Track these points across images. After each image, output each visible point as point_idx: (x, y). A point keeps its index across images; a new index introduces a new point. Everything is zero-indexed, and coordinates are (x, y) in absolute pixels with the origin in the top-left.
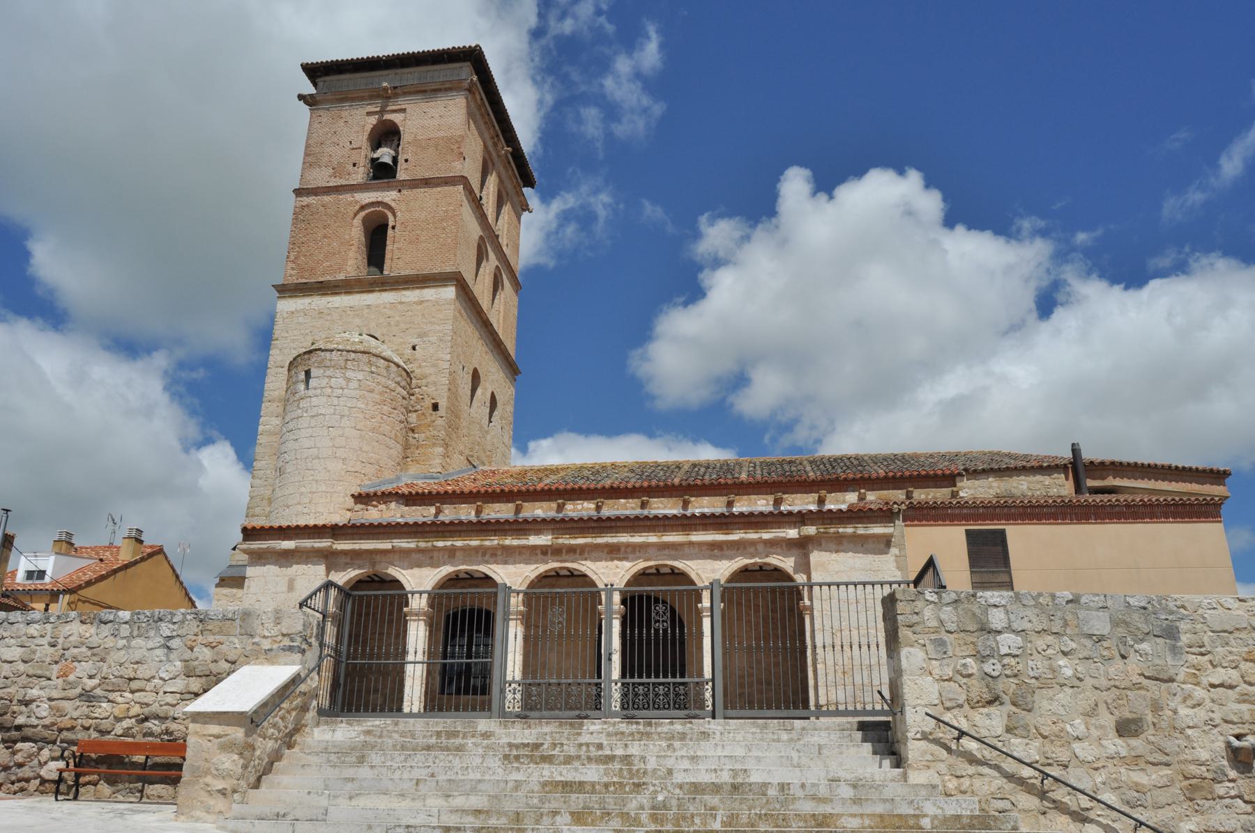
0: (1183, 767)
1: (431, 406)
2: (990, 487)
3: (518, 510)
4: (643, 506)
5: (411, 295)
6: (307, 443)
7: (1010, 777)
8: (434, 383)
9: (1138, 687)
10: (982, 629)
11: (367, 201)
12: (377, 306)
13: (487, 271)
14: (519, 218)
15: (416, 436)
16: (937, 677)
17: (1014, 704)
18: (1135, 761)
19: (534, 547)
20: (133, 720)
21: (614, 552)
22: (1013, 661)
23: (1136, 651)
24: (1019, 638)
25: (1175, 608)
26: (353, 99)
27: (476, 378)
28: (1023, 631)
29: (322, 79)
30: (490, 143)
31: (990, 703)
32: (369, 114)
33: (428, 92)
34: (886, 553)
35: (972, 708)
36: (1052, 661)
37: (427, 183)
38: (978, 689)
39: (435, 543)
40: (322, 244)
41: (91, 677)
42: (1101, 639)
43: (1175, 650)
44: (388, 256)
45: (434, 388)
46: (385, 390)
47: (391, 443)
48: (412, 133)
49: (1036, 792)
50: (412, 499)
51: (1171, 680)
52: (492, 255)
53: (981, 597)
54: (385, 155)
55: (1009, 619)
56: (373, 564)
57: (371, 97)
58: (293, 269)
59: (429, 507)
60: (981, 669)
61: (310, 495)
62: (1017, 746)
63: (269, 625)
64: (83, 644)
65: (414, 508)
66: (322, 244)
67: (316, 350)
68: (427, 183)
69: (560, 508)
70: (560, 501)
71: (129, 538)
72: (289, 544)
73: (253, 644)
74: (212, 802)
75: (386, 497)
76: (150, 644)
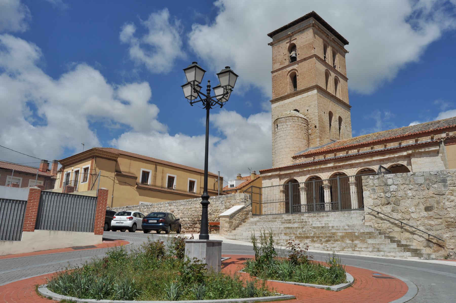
0: (446, 219)
3: (335, 155)
4: (372, 148)
5: (305, 95)
6: (279, 145)
7: (392, 223)
9: (432, 197)
10: (385, 185)
11: (290, 70)
12: (297, 100)
13: (331, 79)
14: (344, 56)
15: (311, 136)
16: (373, 198)
18: (430, 218)
19: (329, 167)
21: (352, 166)
22: (394, 193)
23: (433, 187)
25: (446, 174)
26: (282, 40)
27: (331, 115)
28: (398, 184)
29: (274, 36)
31: (387, 204)
32: (287, 43)
33: (301, 31)
34: (438, 156)
35: (382, 206)
36: (406, 192)
37: (305, 59)
38: (384, 200)
39: (304, 169)
41: (210, 210)
42: (421, 184)
43: (445, 186)
44: (297, 85)
47: (303, 140)
49: (400, 227)
50: (307, 156)
51: (444, 195)
54: (293, 54)
55: (393, 181)
56: (290, 177)
57: (287, 38)
58: (274, 95)
60: (385, 196)
62: (395, 215)
63: (238, 197)
65: (308, 158)
68: (305, 59)
69: (347, 153)
70: (347, 151)
71: (253, 174)
72: (270, 174)
74: (225, 233)
75: (300, 156)
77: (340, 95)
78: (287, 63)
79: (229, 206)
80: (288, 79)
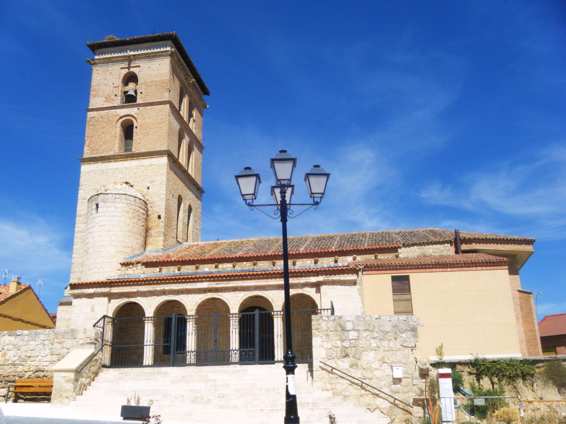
1: (157, 216)
2: (415, 252)
8: (158, 206)
10: (344, 330)
11: (123, 114)
12: (130, 168)
16: (326, 348)
17: (354, 357)
20: (32, 372)
21: (235, 289)
22: (354, 341)
23: (401, 337)
24: (357, 333)
27: (180, 200)
30: (183, 79)
35: (338, 359)
37: (152, 104)
40: (102, 137)
41: (14, 356)
45: (158, 208)
46: (134, 211)
47: (138, 236)
48: (143, 78)
52: (186, 137)
53: (344, 318)
55: (354, 326)
59: (156, 268)
60: (342, 345)
61: (100, 264)
64: (10, 344)
65: (149, 268)
66: (102, 137)
67: (101, 194)
73: (76, 342)
76: (37, 343)
77: (192, 171)
78: (118, 102)
79: (61, 350)
80: (117, 129)
